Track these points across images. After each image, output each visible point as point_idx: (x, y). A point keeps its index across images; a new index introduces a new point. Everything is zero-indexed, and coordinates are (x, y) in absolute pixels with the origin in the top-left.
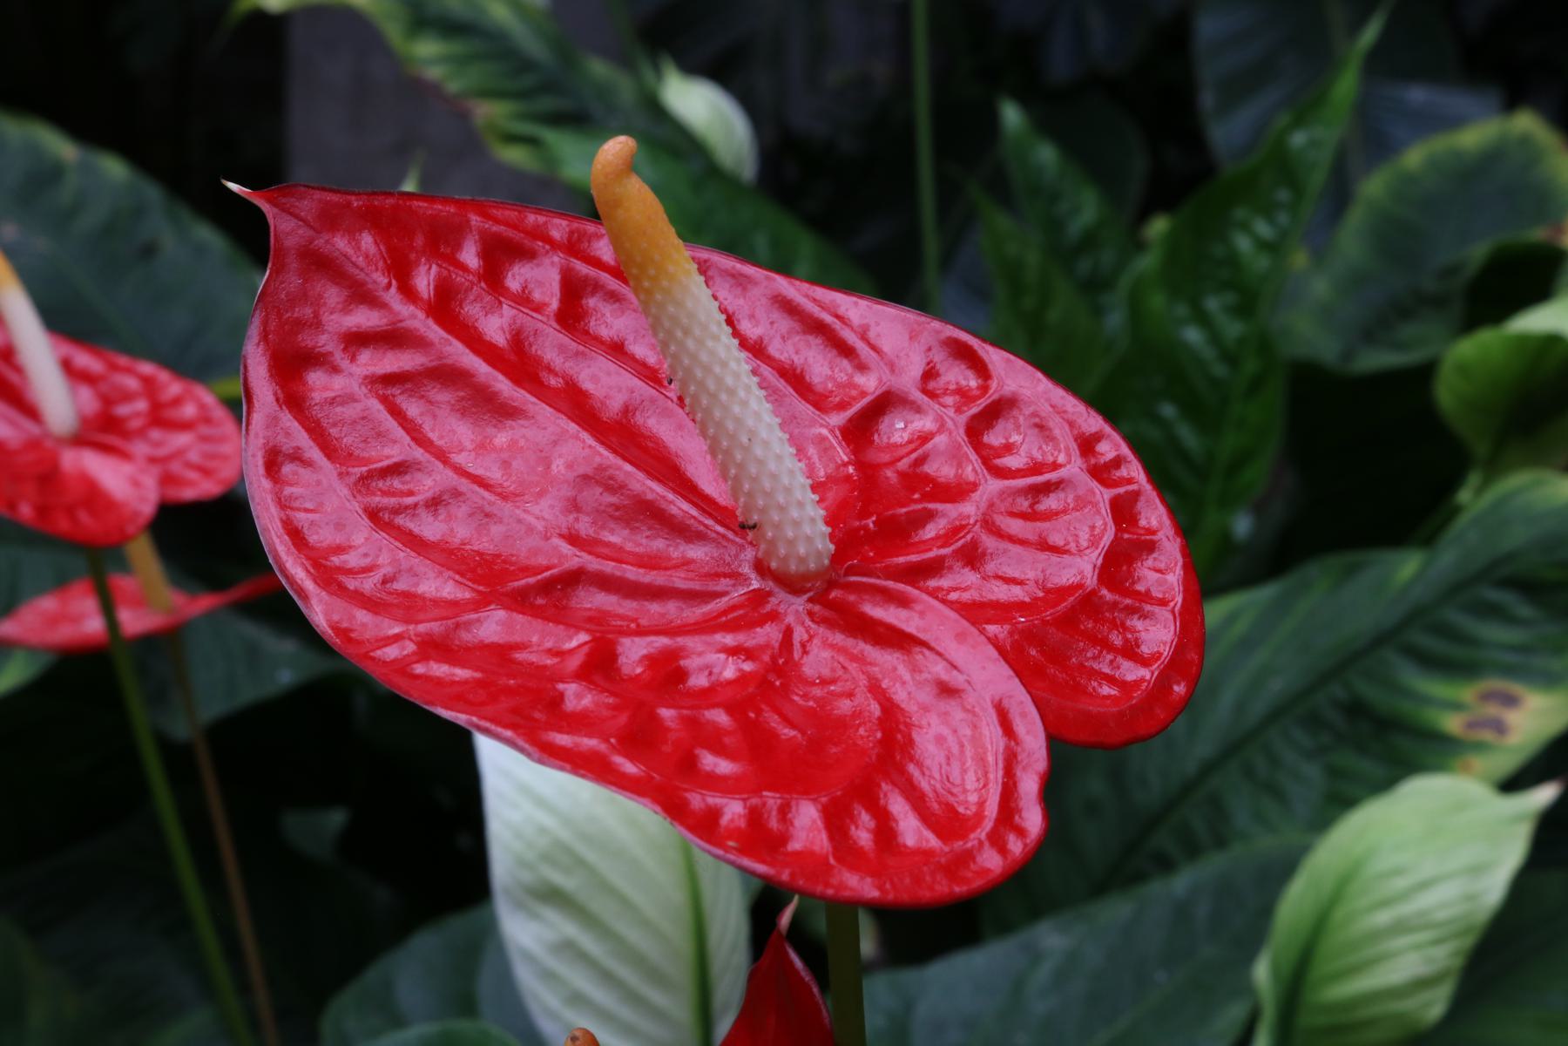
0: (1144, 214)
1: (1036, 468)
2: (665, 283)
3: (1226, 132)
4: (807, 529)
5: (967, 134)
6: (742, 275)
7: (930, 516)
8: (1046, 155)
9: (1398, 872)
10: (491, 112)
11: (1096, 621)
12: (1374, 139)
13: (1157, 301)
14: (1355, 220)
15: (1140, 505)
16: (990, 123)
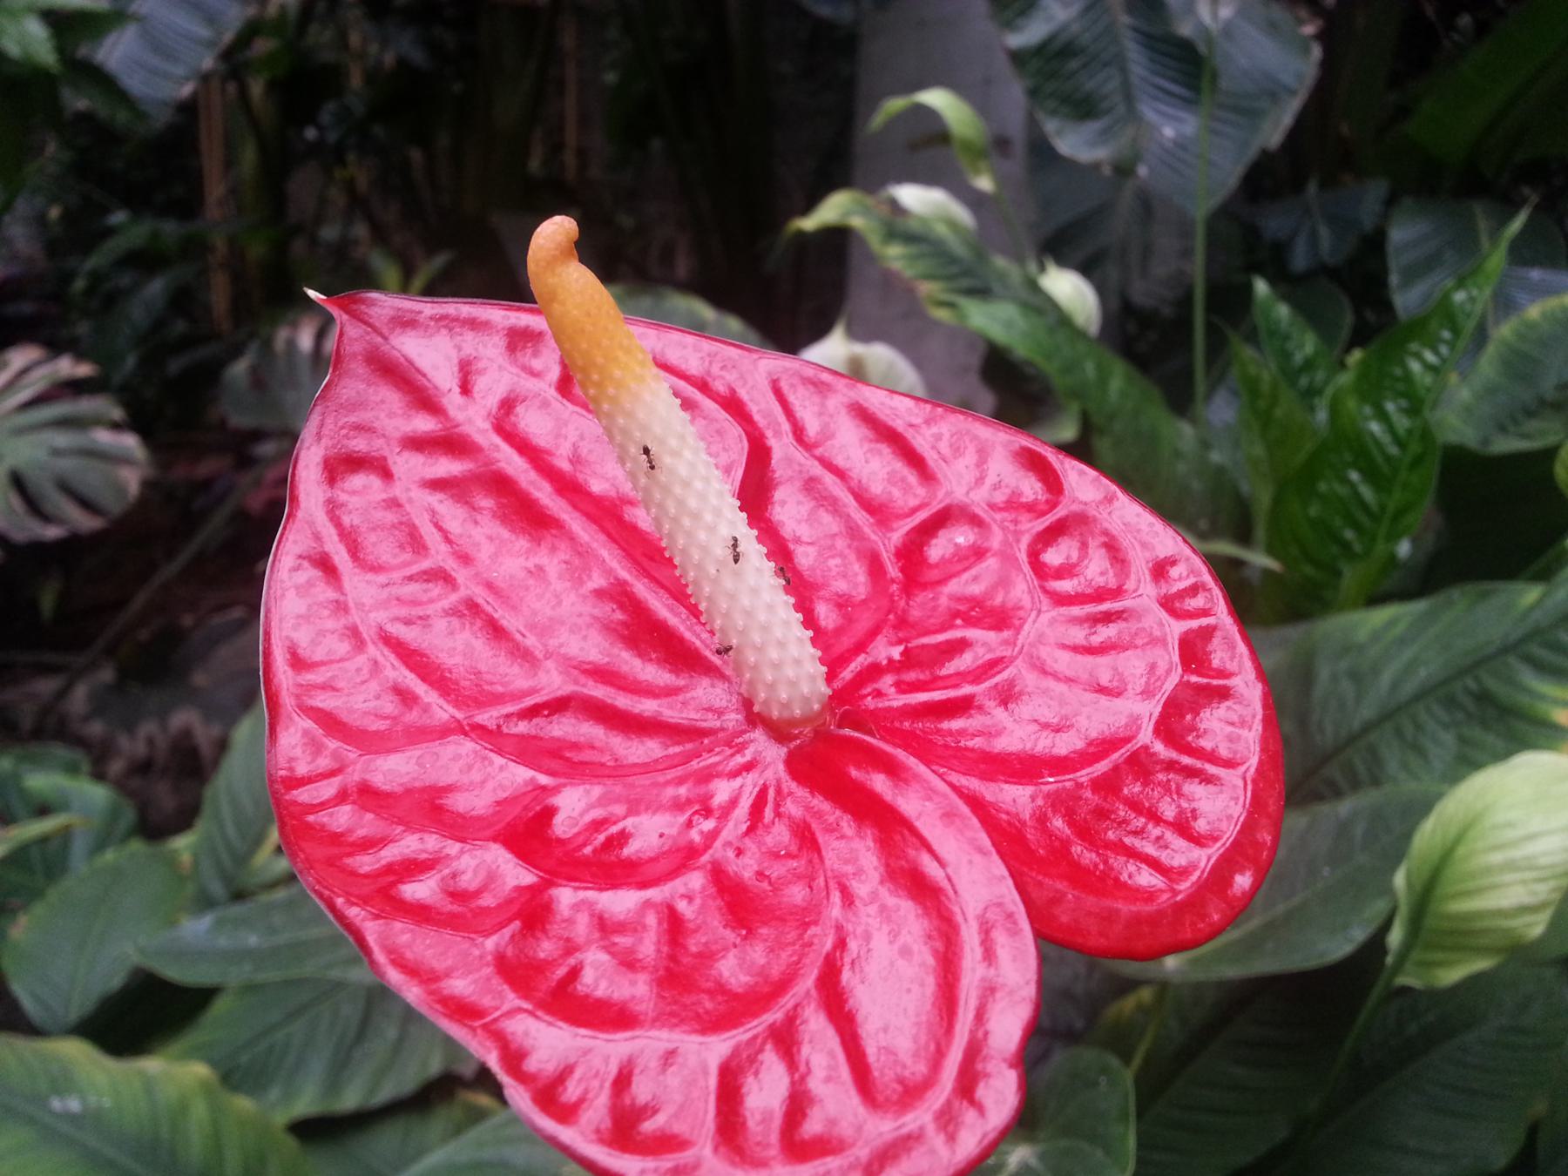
0: (1348, 349)
1: (1100, 595)
2: (611, 391)
3: (1406, 300)
4: (790, 672)
5: (1230, 303)
6: (823, 383)
7: (961, 645)
8: (1283, 311)
9: (1510, 825)
10: (928, 289)
11: (1145, 784)
12: (1505, 304)
13: (1351, 404)
14: (1491, 350)
15: (1216, 642)
16: (1248, 289)
